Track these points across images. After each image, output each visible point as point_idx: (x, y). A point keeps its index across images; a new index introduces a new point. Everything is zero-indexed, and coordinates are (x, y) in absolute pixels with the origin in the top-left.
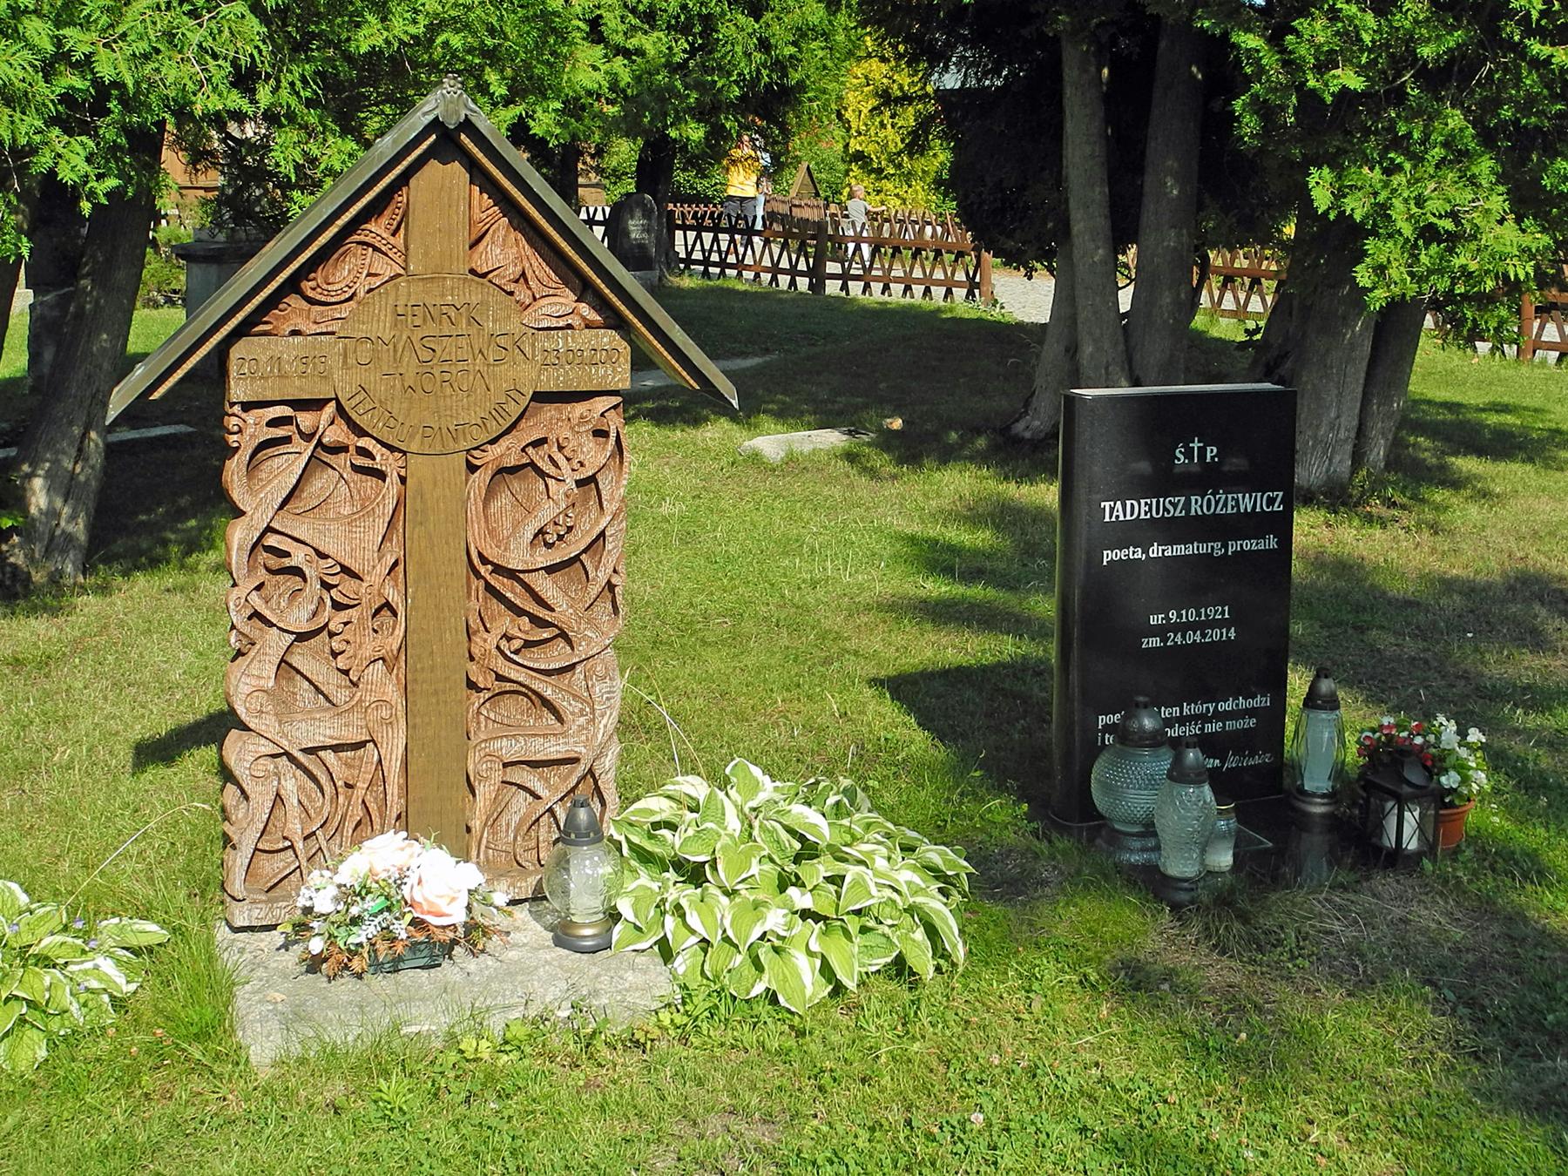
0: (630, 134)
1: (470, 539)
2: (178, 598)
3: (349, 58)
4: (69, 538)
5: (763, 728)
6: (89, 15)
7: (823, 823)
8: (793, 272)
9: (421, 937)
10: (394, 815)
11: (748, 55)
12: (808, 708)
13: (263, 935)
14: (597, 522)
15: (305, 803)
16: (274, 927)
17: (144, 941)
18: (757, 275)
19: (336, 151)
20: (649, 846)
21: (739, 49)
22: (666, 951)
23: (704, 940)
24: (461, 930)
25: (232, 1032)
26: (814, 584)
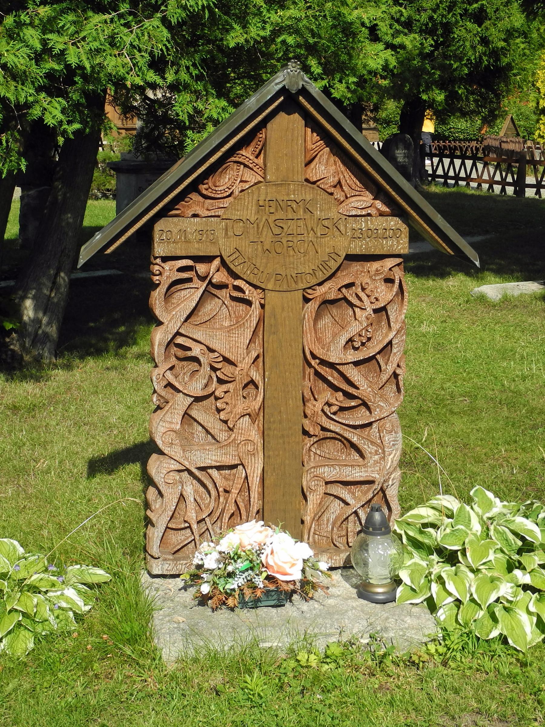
0: (396, 97)
1: (305, 344)
2: (113, 374)
3: (221, 49)
4: (46, 335)
5: (493, 468)
6: (64, 26)
7: (537, 530)
8: (503, 183)
9: (272, 587)
10: (255, 511)
11: (473, 47)
12: (523, 456)
13: (170, 580)
14: (387, 335)
15: (199, 500)
16: (178, 576)
17: (96, 580)
18: (480, 185)
19: (214, 106)
20: (419, 538)
21: (468, 44)
22: (432, 605)
23: (457, 600)
24: (298, 585)
25: (149, 639)
26: (524, 378)
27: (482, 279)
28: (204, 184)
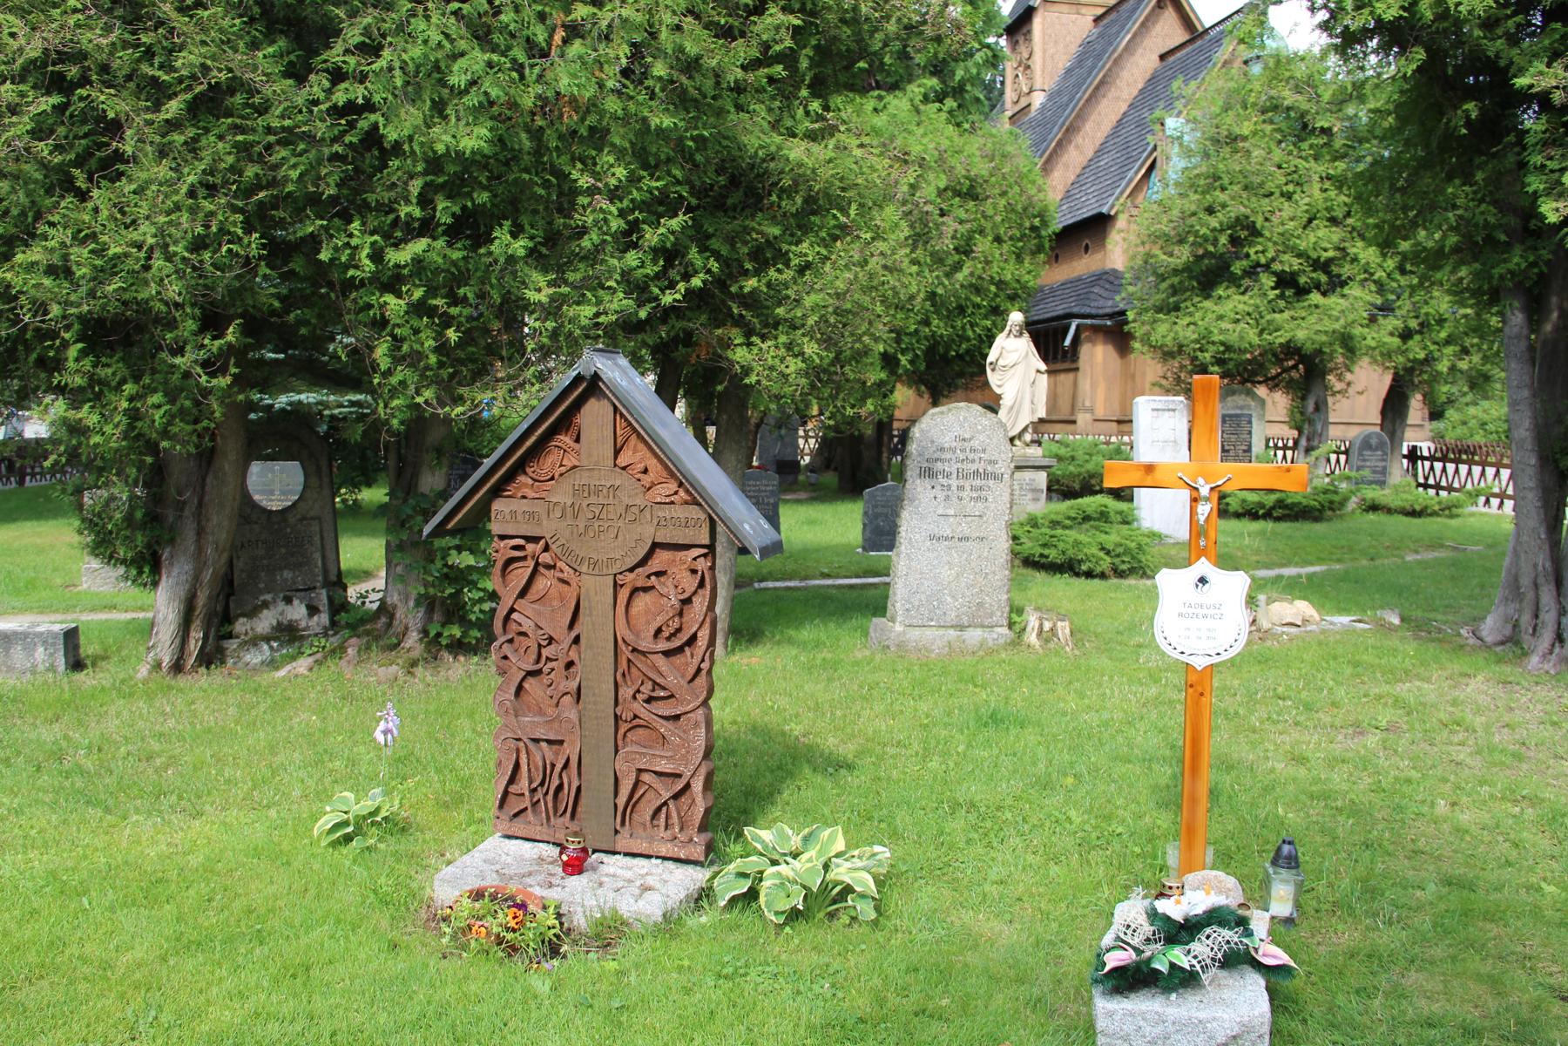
27: (754, 729)
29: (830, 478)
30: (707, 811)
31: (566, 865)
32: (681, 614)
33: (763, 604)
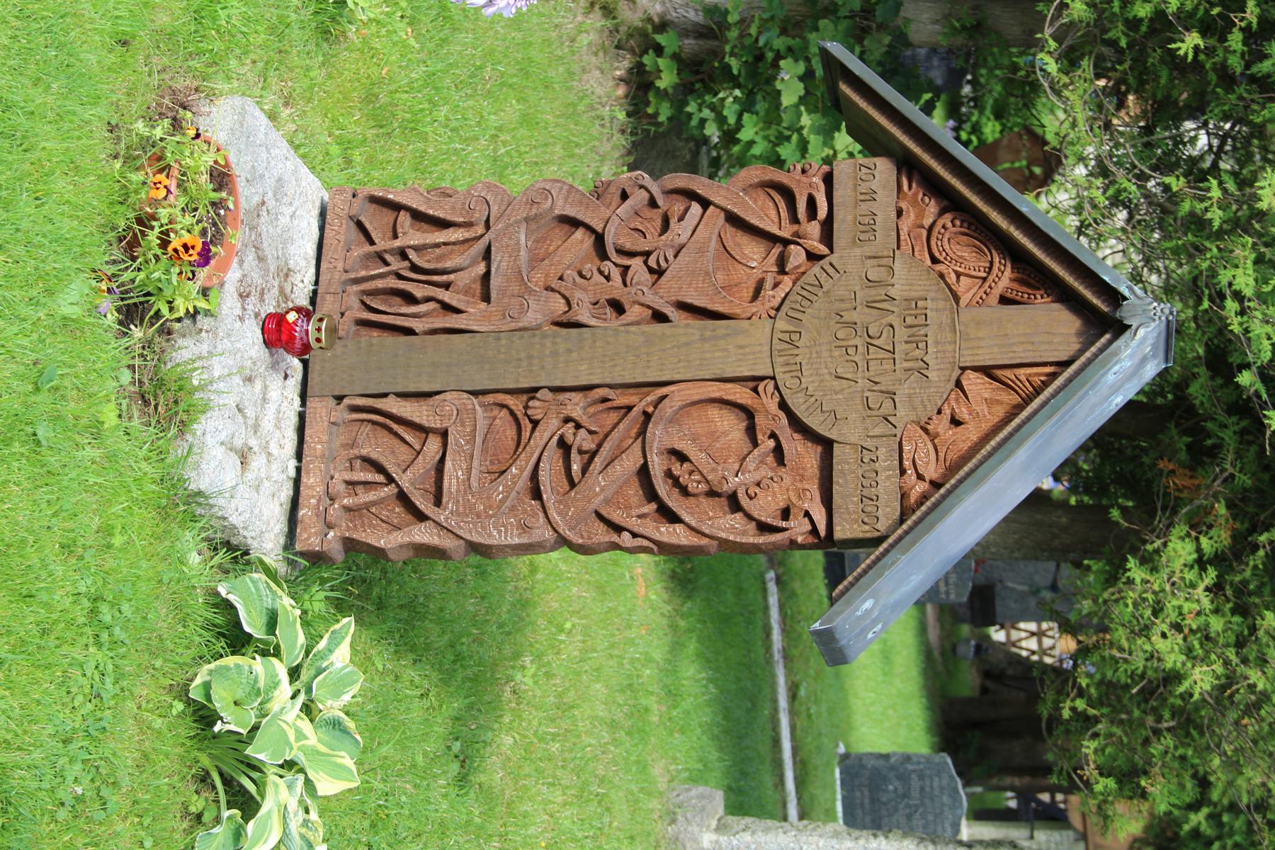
27: (523, 604)
28: (952, 222)
29: (967, 682)
30: (379, 553)
31: (279, 319)
32: (712, 493)
33: (740, 590)
